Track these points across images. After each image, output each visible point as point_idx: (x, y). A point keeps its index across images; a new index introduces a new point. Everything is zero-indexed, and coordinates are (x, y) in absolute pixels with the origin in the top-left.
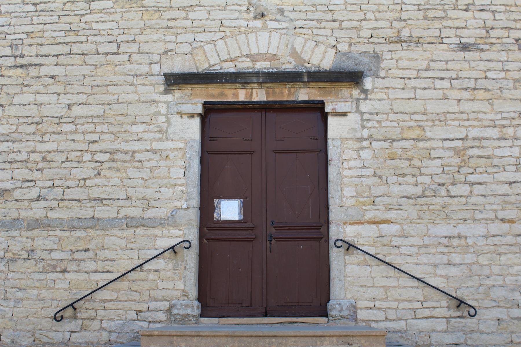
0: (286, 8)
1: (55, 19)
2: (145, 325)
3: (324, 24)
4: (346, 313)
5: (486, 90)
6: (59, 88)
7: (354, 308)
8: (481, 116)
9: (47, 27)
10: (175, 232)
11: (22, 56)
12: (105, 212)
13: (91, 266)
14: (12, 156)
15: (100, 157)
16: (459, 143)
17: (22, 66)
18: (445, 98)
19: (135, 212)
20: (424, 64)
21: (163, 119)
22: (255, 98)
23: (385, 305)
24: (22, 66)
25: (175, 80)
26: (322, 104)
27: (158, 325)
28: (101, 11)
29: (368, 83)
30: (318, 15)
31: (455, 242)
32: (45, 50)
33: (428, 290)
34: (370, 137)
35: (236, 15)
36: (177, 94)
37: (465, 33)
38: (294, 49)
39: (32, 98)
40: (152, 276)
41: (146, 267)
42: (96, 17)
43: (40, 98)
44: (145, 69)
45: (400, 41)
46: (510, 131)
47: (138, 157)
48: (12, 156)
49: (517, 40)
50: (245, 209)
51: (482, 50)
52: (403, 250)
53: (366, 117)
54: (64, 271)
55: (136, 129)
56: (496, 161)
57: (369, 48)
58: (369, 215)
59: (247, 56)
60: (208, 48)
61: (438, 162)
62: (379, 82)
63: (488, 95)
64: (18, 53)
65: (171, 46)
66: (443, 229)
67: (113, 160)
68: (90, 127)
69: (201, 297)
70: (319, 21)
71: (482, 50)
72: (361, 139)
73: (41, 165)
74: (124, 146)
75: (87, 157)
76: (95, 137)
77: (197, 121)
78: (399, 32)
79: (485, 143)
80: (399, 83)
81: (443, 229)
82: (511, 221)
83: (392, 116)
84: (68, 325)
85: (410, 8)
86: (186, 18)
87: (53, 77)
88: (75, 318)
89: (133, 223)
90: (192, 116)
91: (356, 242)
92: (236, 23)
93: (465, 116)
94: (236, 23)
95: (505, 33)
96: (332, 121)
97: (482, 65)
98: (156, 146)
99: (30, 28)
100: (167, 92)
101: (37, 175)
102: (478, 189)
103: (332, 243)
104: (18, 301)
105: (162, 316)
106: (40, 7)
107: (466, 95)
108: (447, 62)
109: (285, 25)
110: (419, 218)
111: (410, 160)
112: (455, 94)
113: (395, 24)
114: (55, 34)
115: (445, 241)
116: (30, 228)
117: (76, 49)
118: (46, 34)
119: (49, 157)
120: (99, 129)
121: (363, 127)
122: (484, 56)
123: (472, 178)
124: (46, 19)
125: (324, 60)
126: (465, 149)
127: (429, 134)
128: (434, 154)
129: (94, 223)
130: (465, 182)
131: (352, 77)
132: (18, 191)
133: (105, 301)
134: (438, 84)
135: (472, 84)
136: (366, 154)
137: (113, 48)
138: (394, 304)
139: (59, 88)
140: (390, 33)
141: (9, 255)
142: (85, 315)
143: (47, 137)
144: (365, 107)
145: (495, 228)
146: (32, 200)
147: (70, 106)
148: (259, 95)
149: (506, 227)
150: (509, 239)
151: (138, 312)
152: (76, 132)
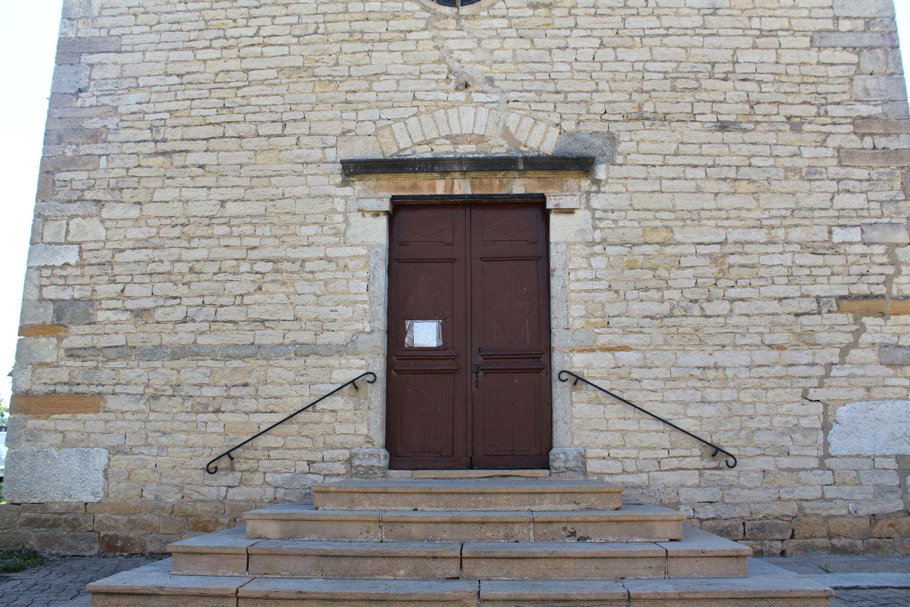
0: (496, 76)
1: (205, 93)
2: (319, 479)
3: (544, 96)
4: (572, 464)
5: (750, 181)
6: (210, 180)
7: (583, 458)
8: (743, 214)
9: (196, 103)
10: (356, 362)
11: (165, 141)
13: (251, 404)
14: (152, 266)
15: (261, 267)
16: (716, 249)
17: (164, 153)
18: (699, 190)
19: (305, 337)
20: (672, 148)
21: (339, 218)
22: (457, 191)
23: (622, 453)
24: (164, 153)
25: (355, 169)
27: (335, 480)
28: (262, 82)
29: (601, 172)
30: (536, 86)
31: (711, 374)
32: (192, 132)
33: (676, 434)
34: (603, 241)
35: (433, 85)
36: (358, 186)
37: (724, 108)
38: (506, 129)
39: (175, 193)
40: (327, 418)
41: (319, 406)
42: (255, 90)
43: (187, 194)
44: (317, 154)
46: (780, 233)
47: (309, 266)
48: (152, 266)
49: (789, 118)
51: (745, 131)
52: (646, 384)
53: (598, 214)
54: (217, 411)
55: (306, 231)
56: (762, 272)
57: (602, 127)
58: (603, 340)
59: (447, 137)
60: (397, 127)
61: (689, 273)
62: (615, 171)
63: (752, 188)
64: (159, 137)
65: (350, 126)
66: (696, 358)
67: (277, 271)
68: (248, 229)
69: (389, 445)
70: (539, 92)
71: (745, 131)
72: (593, 243)
73: (188, 278)
74: (291, 253)
75: (245, 267)
76: (254, 242)
77: (383, 221)
78: (640, 107)
79: (749, 248)
80: (641, 172)
81: (696, 358)
82: (781, 348)
83: (631, 214)
85: (654, 76)
86: (370, 90)
87: (202, 167)
88: (233, 469)
89: (303, 350)
90: (377, 214)
91: (586, 374)
92: (432, 96)
93: (723, 214)
94: (432, 96)
95: (773, 109)
96: (554, 219)
98: (332, 252)
99: (174, 106)
100: (345, 183)
101: (182, 290)
102: (740, 307)
103: (555, 376)
104: (162, 448)
105: (340, 468)
106: (186, 79)
107: (725, 187)
108: (701, 144)
109: (495, 98)
110: (666, 343)
111: (655, 269)
113: (635, 96)
114: (205, 112)
115: (698, 373)
116: (175, 357)
117: (230, 131)
118: (194, 113)
119: (198, 267)
120: (259, 231)
121: (595, 228)
122: (748, 137)
123: (732, 293)
125: (544, 141)
126: (724, 256)
127: (678, 237)
128: (685, 262)
129: (254, 351)
130: (724, 298)
131: (582, 165)
132: (160, 311)
133: (269, 449)
134: (690, 173)
135: (732, 174)
136: (598, 262)
138: (633, 453)
139: (210, 180)
140: (629, 108)
141: (150, 391)
142: (245, 466)
143: (195, 242)
144: (597, 202)
145: (761, 356)
146: (176, 322)
147: (223, 203)
148: (462, 187)
150: (778, 370)
151: (310, 463)
152: (230, 235)
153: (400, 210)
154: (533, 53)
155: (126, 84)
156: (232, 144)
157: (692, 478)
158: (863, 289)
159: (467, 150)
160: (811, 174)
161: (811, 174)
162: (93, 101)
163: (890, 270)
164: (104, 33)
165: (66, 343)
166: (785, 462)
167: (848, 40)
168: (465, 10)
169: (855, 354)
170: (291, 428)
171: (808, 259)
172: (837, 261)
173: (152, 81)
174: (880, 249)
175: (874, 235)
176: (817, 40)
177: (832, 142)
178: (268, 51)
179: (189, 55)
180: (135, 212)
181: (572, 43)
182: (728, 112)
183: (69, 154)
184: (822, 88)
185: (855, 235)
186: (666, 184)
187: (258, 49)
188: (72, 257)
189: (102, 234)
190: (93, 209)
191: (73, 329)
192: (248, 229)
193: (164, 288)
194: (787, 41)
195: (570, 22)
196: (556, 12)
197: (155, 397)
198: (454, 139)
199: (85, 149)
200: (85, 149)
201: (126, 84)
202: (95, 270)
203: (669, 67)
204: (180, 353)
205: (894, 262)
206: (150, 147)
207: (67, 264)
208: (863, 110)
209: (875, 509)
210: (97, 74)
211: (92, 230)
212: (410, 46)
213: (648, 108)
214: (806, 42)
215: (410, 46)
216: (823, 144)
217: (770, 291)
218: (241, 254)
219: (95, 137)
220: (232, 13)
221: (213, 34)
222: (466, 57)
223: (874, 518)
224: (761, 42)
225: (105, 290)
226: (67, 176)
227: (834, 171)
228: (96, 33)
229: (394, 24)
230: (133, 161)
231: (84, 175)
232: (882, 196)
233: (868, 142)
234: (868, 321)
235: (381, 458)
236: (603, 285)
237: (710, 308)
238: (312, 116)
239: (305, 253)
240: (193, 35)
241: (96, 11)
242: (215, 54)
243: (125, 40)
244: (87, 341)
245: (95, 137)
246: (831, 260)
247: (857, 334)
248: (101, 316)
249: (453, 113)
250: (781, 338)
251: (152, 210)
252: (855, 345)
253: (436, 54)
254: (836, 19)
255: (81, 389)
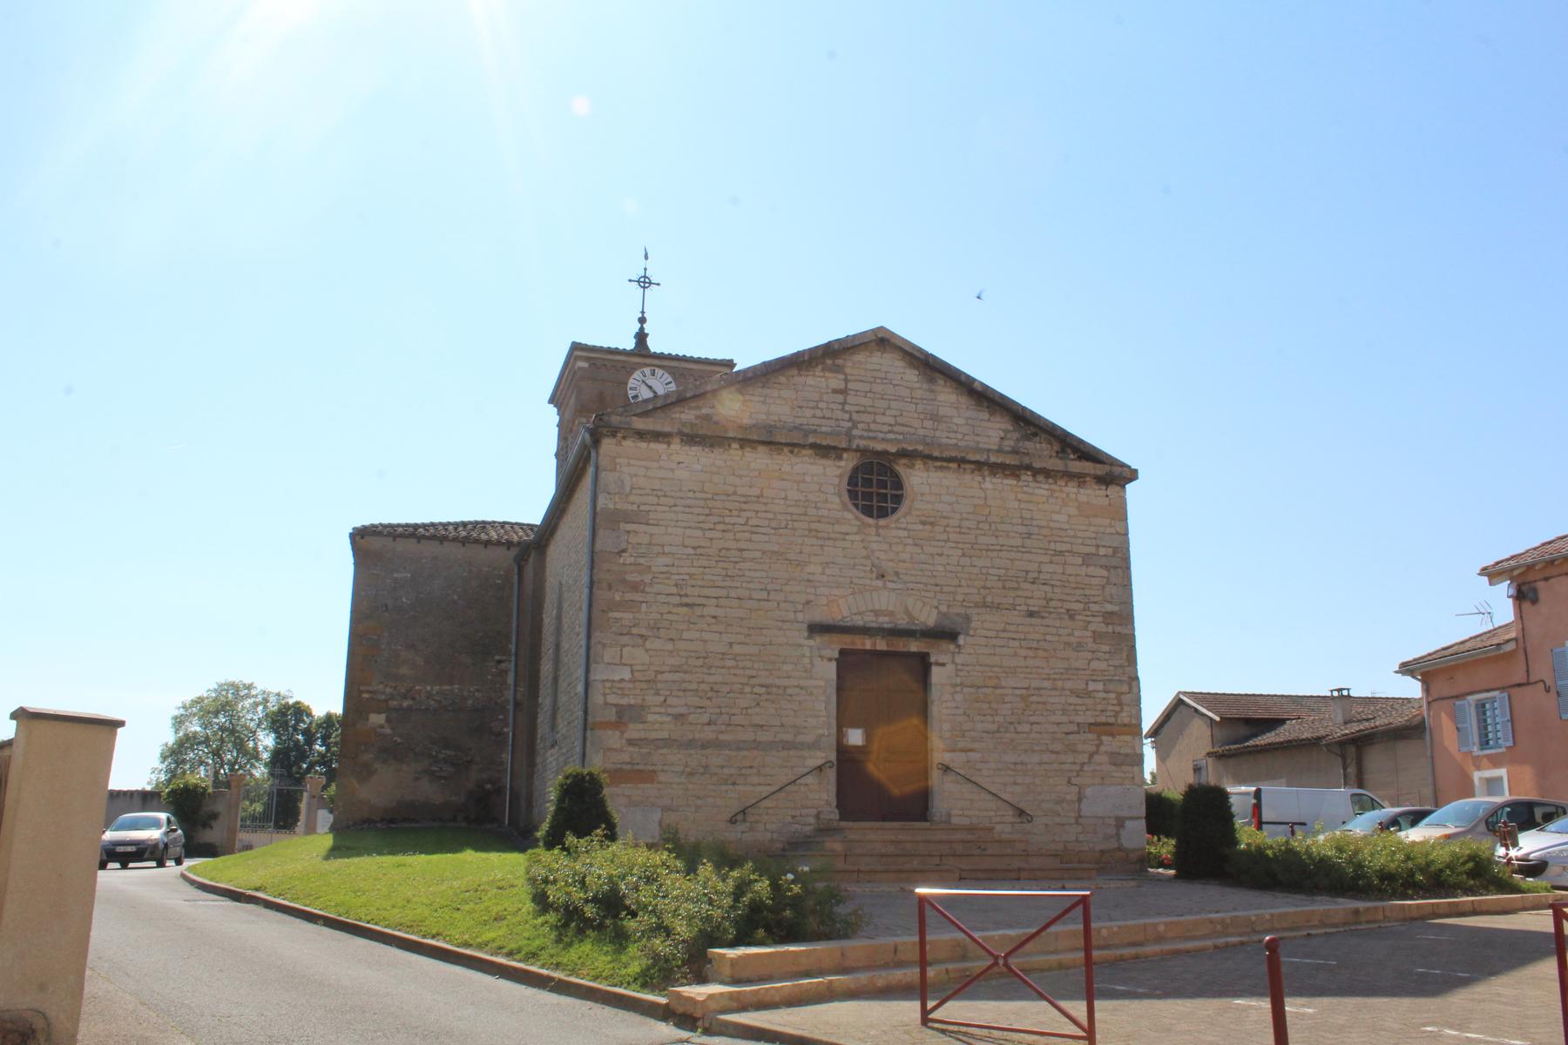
6: (721, 628)
7: (949, 815)
10: (819, 754)
12: (764, 737)
13: (756, 780)
14: (684, 685)
16: (1024, 692)
17: (687, 605)
18: (1016, 654)
19: (788, 737)
20: (1001, 627)
21: (806, 661)
24: (687, 605)
25: (816, 629)
26: (927, 654)
28: (752, 560)
29: (961, 640)
30: (924, 580)
32: (706, 592)
36: (818, 640)
37: (1031, 602)
39: (697, 635)
40: (803, 789)
42: (748, 565)
43: (706, 636)
44: (791, 616)
45: (985, 605)
46: (1059, 684)
47: (789, 691)
50: (854, 726)
52: (985, 772)
55: (787, 667)
57: (962, 611)
58: (961, 745)
60: (841, 601)
62: (969, 639)
65: (812, 598)
69: (840, 805)
74: (777, 682)
75: (747, 689)
76: (753, 673)
77: (834, 665)
80: (983, 641)
84: (741, 827)
89: (787, 746)
92: (861, 581)
96: (935, 670)
97: (1043, 629)
98: (802, 683)
99: (692, 570)
100: (809, 637)
101: (708, 703)
102: (1036, 728)
104: (698, 807)
105: (812, 820)
106: (699, 551)
107: (1031, 653)
112: (1023, 652)
122: (1045, 622)
123: (1032, 719)
124: (706, 563)
125: (928, 618)
129: (756, 745)
131: (951, 636)
134: (1011, 643)
135: (1034, 645)
136: (959, 697)
137: (764, 595)
139: (721, 628)
140: (978, 599)
144: (959, 659)
145: (1046, 757)
147: (731, 644)
148: (881, 645)
149: (1053, 757)
150: (1055, 766)
152: (737, 667)
153: (848, 662)
154: (923, 557)
155: (656, 549)
156: (735, 603)
157: (1008, 828)
158: (1102, 719)
159: (884, 621)
160: (1079, 647)
161: (1079, 647)
162: (632, 560)
163: (1117, 708)
164: (635, 507)
165: (626, 735)
166: (1058, 820)
167: (1104, 561)
168: (882, 522)
169: (1097, 758)
170: (782, 795)
171: (1073, 700)
172: (1088, 701)
173: (673, 550)
174: (1113, 696)
175: (1111, 687)
176: (1087, 559)
177: (1091, 627)
178: (755, 537)
179: (699, 533)
180: (669, 646)
181: (946, 551)
182: (1035, 605)
183: (617, 598)
184: (1087, 592)
185: (1100, 686)
186: (998, 650)
187: (747, 535)
188: (627, 675)
189: (646, 659)
190: (640, 641)
191: (631, 726)
192: (748, 664)
193: (695, 701)
194: (1070, 559)
195: (945, 537)
196: (937, 529)
197: (692, 774)
198: (876, 613)
199: (629, 596)
200: (629, 596)
201: (656, 549)
202: (644, 686)
203: (1002, 572)
204: (705, 745)
205: (1120, 704)
206: (676, 600)
207: (622, 680)
208: (1109, 608)
209: (1103, 847)
210: (633, 539)
211: (639, 656)
212: (848, 544)
213: (989, 599)
214: (1080, 560)
215: (848, 544)
216: (1086, 629)
217: (1053, 719)
218: (745, 680)
219: (635, 587)
220: (729, 505)
221: (716, 519)
222: (883, 556)
223: (1102, 852)
224: (1055, 559)
225: (651, 699)
226: (618, 615)
227: (1091, 646)
228: (630, 507)
229: (837, 528)
230: (665, 609)
231: (630, 616)
232: (1116, 663)
233: (1110, 629)
234: (1104, 738)
235: (835, 815)
236: (961, 711)
237: (1020, 728)
238: (787, 588)
239: (786, 682)
240: (702, 518)
241: (628, 489)
242: (719, 535)
243: (652, 515)
244: (642, 735)
245: (635, 587)
246: (1087, 701)
247: (1098, 746)
248: (650, 718)
249: (875, 594)
250: (1058, 747)
251: (681, 645)
252: (1097, 752)
253: (864, 553)
254: (1098, 546)
255: (640, 767)
